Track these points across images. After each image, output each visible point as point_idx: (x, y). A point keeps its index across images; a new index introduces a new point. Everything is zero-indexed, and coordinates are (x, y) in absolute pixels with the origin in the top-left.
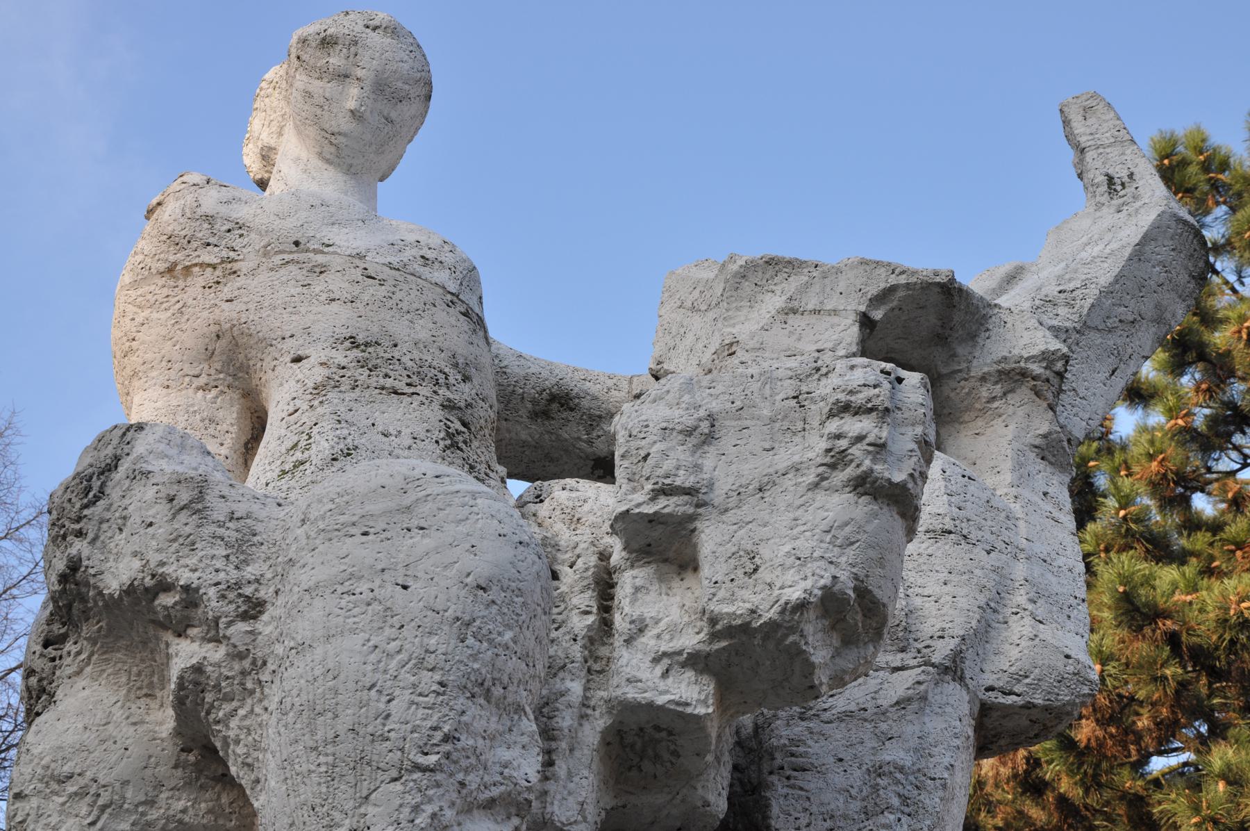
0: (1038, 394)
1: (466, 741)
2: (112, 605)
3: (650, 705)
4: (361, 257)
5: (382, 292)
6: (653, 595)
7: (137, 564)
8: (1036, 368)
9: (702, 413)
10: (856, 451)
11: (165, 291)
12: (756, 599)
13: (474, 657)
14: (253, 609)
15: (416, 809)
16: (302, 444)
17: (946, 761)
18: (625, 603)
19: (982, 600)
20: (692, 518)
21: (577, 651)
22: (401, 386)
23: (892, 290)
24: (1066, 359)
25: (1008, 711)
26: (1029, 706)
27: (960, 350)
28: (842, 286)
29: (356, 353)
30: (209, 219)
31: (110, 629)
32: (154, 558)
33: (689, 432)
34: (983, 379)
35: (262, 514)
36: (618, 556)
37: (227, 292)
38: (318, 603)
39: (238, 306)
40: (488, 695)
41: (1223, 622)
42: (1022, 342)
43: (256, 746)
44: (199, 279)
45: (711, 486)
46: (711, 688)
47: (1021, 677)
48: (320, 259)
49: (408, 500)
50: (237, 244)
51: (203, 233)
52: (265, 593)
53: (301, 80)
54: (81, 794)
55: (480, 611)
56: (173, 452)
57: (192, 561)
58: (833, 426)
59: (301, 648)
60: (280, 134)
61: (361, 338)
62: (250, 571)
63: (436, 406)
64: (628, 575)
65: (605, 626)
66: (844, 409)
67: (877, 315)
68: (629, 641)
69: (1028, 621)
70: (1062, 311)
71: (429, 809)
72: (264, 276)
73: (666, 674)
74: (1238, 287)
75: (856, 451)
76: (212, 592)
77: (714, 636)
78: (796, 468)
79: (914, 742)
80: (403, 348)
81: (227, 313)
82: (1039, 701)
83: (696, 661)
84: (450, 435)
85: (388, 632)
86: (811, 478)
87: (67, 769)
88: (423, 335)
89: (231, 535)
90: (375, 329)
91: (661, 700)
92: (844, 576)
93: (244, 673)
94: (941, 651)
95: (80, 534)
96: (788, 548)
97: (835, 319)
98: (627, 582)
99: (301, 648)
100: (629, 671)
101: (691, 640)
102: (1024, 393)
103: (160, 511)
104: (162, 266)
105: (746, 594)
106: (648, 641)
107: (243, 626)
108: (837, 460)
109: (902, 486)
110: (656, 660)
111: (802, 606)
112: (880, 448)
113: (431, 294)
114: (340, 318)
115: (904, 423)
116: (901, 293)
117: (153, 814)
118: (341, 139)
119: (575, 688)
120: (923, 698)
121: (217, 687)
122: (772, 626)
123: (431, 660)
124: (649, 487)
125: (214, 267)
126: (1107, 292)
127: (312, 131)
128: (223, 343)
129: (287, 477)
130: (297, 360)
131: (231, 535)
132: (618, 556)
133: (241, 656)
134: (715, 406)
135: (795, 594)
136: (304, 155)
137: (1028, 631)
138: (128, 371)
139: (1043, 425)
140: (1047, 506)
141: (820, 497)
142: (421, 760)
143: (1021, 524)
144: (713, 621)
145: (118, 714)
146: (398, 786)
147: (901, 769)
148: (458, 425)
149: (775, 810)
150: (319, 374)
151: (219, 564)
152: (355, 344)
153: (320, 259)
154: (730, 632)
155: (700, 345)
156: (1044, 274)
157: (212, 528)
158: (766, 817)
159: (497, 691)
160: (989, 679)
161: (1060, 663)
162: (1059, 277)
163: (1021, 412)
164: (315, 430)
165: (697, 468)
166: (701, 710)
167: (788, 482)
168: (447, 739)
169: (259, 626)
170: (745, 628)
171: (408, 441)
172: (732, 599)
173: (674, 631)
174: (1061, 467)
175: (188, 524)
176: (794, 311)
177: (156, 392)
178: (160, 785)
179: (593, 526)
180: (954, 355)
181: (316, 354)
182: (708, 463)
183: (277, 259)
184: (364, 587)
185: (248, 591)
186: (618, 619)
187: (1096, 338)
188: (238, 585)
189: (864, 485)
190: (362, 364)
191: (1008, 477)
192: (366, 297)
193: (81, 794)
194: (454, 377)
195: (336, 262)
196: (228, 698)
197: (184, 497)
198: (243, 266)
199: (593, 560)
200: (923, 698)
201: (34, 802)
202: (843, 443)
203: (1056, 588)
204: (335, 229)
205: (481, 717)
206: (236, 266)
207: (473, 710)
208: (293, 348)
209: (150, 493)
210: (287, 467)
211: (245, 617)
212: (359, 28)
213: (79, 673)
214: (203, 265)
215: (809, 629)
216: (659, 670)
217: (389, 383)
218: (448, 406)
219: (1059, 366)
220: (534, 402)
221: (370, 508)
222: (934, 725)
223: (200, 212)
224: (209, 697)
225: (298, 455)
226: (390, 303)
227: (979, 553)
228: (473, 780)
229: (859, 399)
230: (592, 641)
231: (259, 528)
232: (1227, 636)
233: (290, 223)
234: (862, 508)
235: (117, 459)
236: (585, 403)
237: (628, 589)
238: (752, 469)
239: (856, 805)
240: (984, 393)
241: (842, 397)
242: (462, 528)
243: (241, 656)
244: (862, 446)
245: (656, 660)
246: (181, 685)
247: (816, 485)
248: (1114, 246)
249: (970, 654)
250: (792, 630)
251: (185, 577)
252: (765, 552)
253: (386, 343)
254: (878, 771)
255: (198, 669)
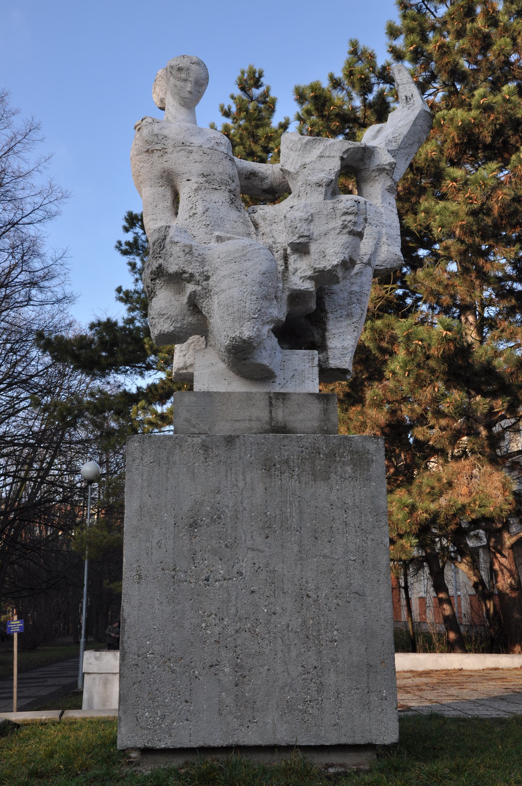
0: (388, 174)
1: (263, 310)
2: (170, 275)
3: (300, 290)
4: (201, 147)
5: (208, 158)
6: (298, 262)
7: (177, 267)
8: (387, 167)
9: (309, 214)
10: (349, 225)
11: (147, 158)
12: (326, 264)
13: (264, 291)
14: (207, 278)
15: (254, 327)
16: (194, 207)
17: (367, 288)
18: (292, 264)
19: (375, 242)
20: (308, 243)
21: (280, 276)
22: (217, 187)
23: (349, 149)
24: (395, 164)
25: (381, 270)
26: (386, 268)
27: (367, 162)
28: (335, 148)
29: (204, 179)
30: (157, 135)
31: (169, 279)
32: (182, 266)
33: (306, 220)
34: (373, 171)
35: (206, 253)
36: (289, 251)
37: (165, 158)
38: (226, 280)
39: (169, 163)
40: (266, 299)
41: (426, 159)
42: (384, 159)
43: (210, 309)
44: (157, 154)
45: (313, 234)
46: (314, 284)
47: (384, 262)
48: (190, 148)
49: (244, 253)
50: (166, 143)
51: (156, 140)
52: (210, 274)
53: (172, 80)
54: (168, 318)
55: (264, 279)
56: (179, 234)
57: (191, 267)
58: (343, 218)
59: (223, 291)
60: (166, 94)
61: (205, 174)
62: (205, 268)
63: (227, 192)
64: (292, 256)
65: (287, 268)
66: (346, 213)
67: (345, 156)
68: (294, 274)
69: (386, 246)
70: (393, 144)
71: (256, 327)
72: (175, 154)
73: (303, 282)
74: (435, 13)
75: (349, 225)
76: (197, 274)
77: (315, 272)
78: (334, 229)
79: (359, 284)
80: (217, 175)
81: (166, 165)
82: (389, 267)
83: (310, 278)
84: (231, 200)
85: (243, 287)
86: (338, 231)
87: (164, 312)
88: (221, 170)
89: (200, 260)
90: (209, 170)
91: (302, 288)
92: (346, 256)
93: (206, 293)
94: (366, 259)
95: (160, 257)
96: (333, 250)
97: (334, 159)
98: (292, 258)
99: (223, 291)
100: (294, 282)
101: (309, 273)
102: (384, 174)
103: (181, 254)
104: (145, 150)
105: (323, 262)
106: (298, 273)
107: (205, 282)
108: (345, 227)
109: (361, 232)
110: (300, 278)
111: (337, 266)
112: (355, 223)
113: (222, 156)
114: (198, 168)
115: (360, 215)
116: (351, 150)
117: (185, 322)
118: (186, 100)
119: (281, 285)
120: (362, 272)
121: (200, 296)
122: (329, 270)
123: (254, 293)
124: (297, 235)
125: (160, 150)
126: (405, 137)
127: (177, 97)
128: (166, 173)
129: (192, 218)
130: (188, 180)
131: (200, 260)
132: (289, 251)
133: (205, 289)
134: (312, 211)
135: (335, 263)
136: (175, 104)
137: (386, 249)
138: (139, 181)
139: (389, 183)
140: (390, 207)
141: (340, 236)
142: (254, 316)
143: (384, 215)
144: (315, 269)
145: (173, 299)
146: (249, 323)
147: (357, 292)
148: (233, 196)
149: (326, 305)
150: (195, 186)
151: (198, 267)
152: (204, 176)
153: (190, 148)
154: (319, 271)
155: (294, 162)
156: (388, 131)
157: (195, 258)
158: (324, 307)
159: (269, 297)
160: (377, 263)
161: (394, 256)
162: (393, 132)
163: (383, 180)
164: (197, 203)
165: (309, 229)
166: (312, 290)
167: (332, 232)
168: (259, 311)
169: (209, 282)
170: (323, 271)
171: (221, 204)
172: (319, 264)
173: (305, 271)
174: (393, 193)
175: (188, 257)
176: (322, 157)
177: (148, 188)
178: (185, 315)
179: (270, 220)
180: (365, 163)
181: (194, 179)
182: (312, 227)
183: (178, 149)
184: (236, 276)
185: (205, 274)
186: (290, 268)
187: (402, 151)
188: (203, 272)
189: (351, 233)
190: (207, 182)
191: (380, 201)
192: (205, 160)
193: (168, 318)
194: (230, 181)
195: (195, 149)
196: (202, 298)
197: (187, 250)
198: (169, 150)
199: (282, 251)
200: (362, 272)
201: (157, 320)
202: (346, 223)
203: (393, 234)
204: (193, 137)
205: (266, 304)
206: (167, 150)
207: (264, 303)
208: (186, 176)
209: (178, 249)
210: (191, 214)
211: (205, 280)
212: (189, 64)
213: (161, 288)
214: (157, 150)
215: (338, 270)
216: (301, 281)
217: (214, 187)
218: (230, 191)
219: (393, 166)
220: (246, 175)
221: (236, 255)
222: (364, 279)
223: (154, 133)
224: (197, 298)
225: (193, 211)
226: (211, 161)
227: (374, 227)
228: (265, 318)
229: (350, 211)
230: (283, 272)
231: (206, 257)
232: (427, 164)
233: (180, 137)
234: (351, 237)
235: (165, 236)
236: (260, 174)
237: (293, 261)
238: (323, 229)
239: (346, 302)
240: (374, 174)
241: (345, 210)
242: (258, 259)
243: (205, 289)
244: (351, 223)
245: (300, 278)
246: (190, 294)
247: (339, 233)
248: (407, 121)
249: (372, 258)
250: (334, 271)
251: (190, 271)
252: (327, 251)
253: (212, 175)
254: (351, 293)
255: (195, 292)
